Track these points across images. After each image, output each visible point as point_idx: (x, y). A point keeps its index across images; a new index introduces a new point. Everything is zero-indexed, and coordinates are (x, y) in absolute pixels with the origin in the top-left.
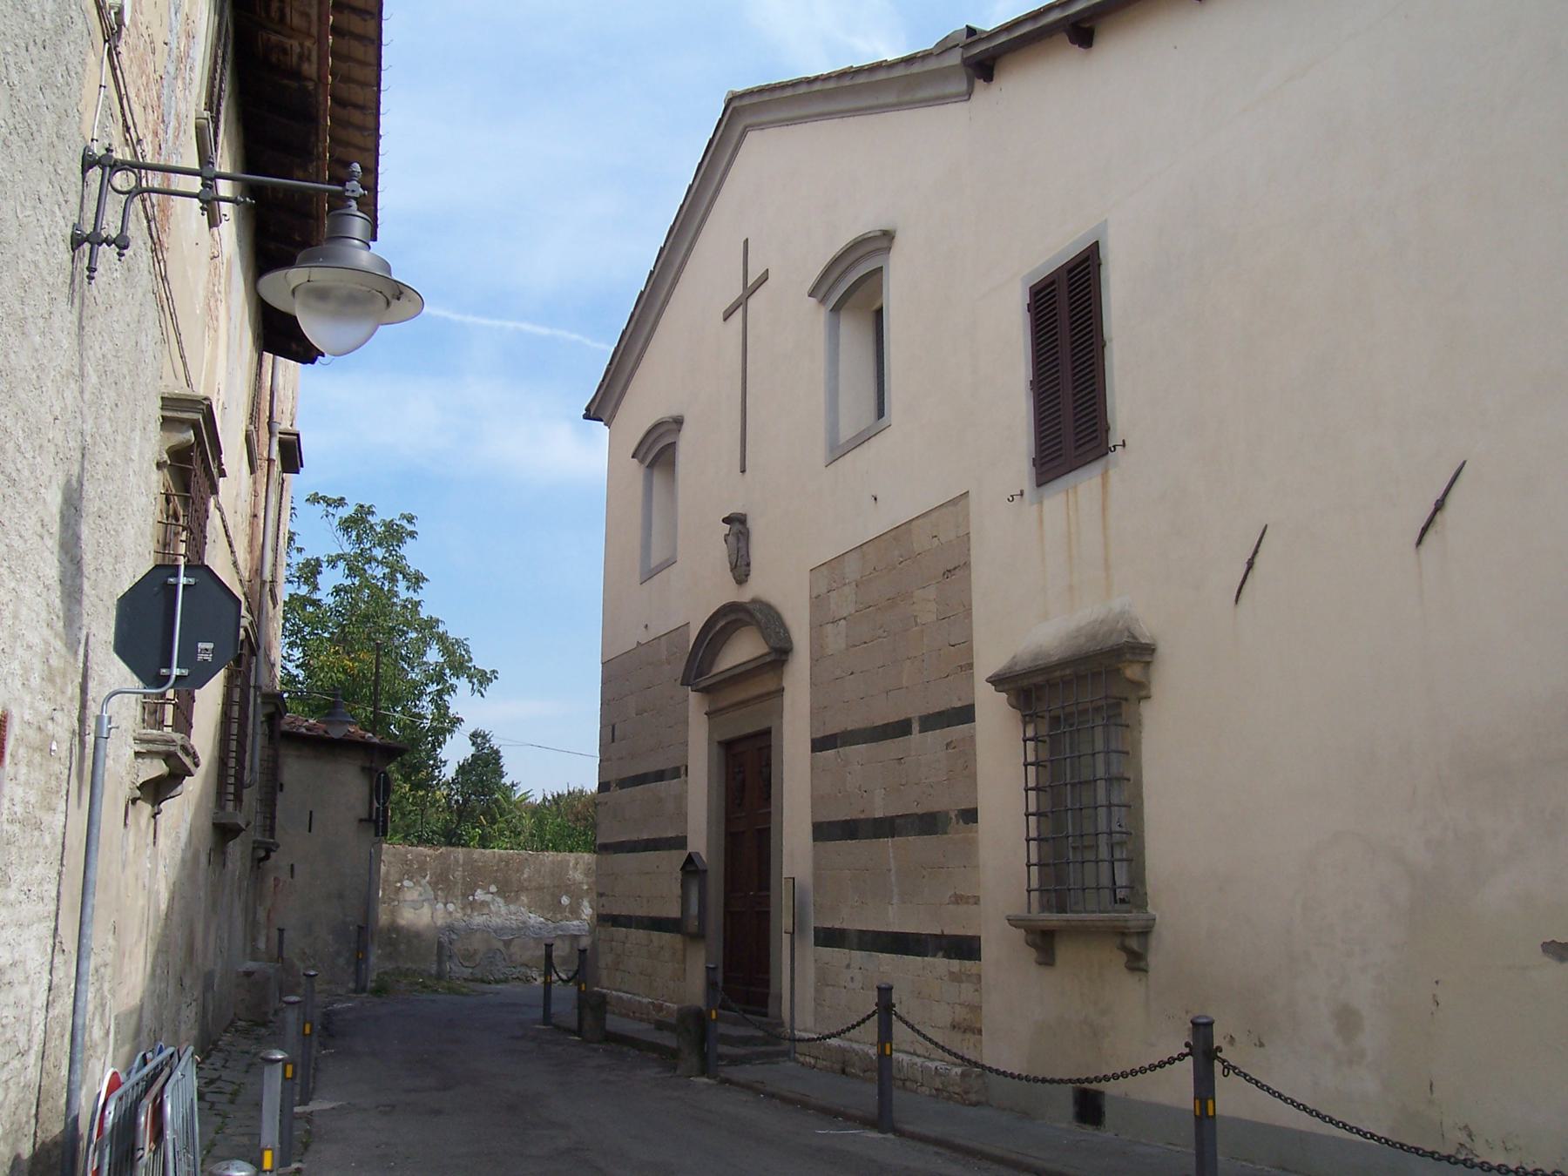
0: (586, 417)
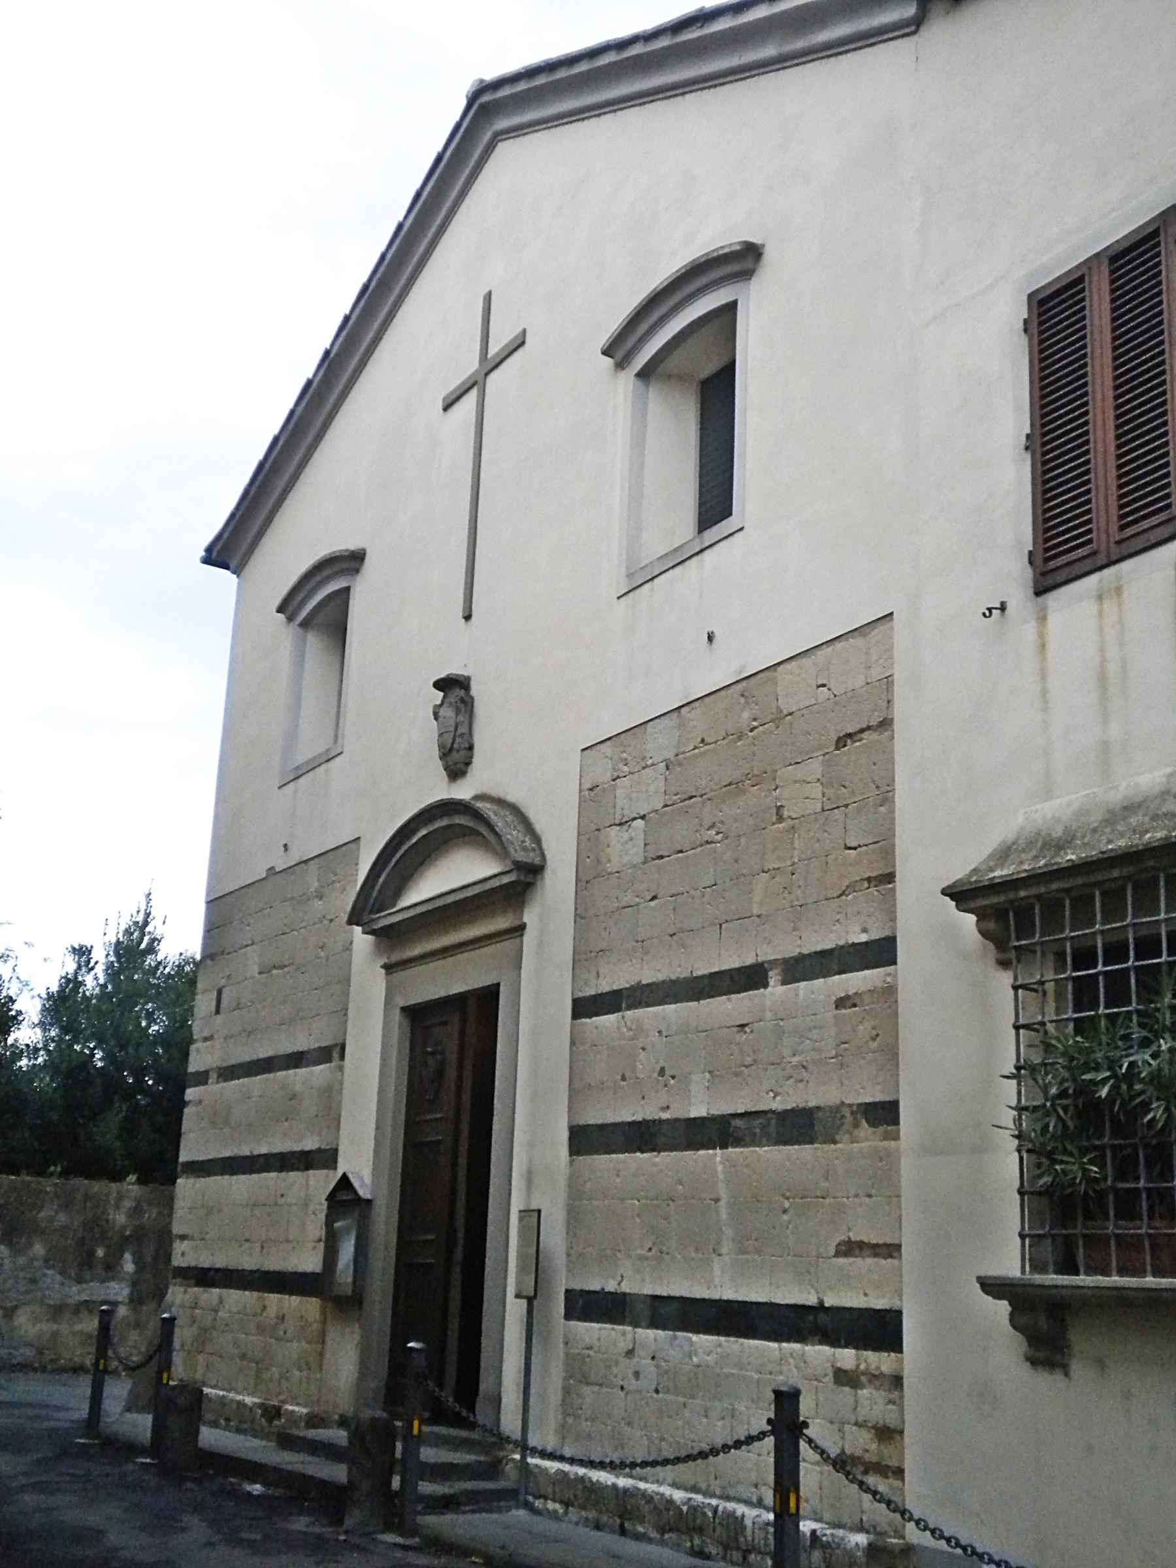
0: (207, 560)
